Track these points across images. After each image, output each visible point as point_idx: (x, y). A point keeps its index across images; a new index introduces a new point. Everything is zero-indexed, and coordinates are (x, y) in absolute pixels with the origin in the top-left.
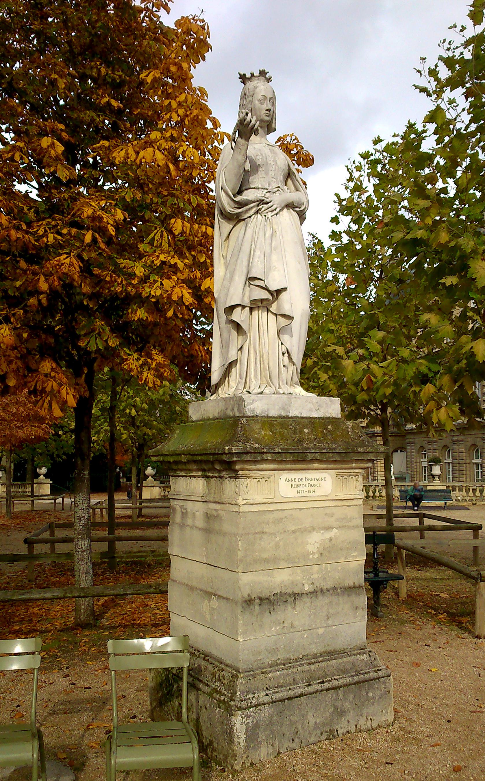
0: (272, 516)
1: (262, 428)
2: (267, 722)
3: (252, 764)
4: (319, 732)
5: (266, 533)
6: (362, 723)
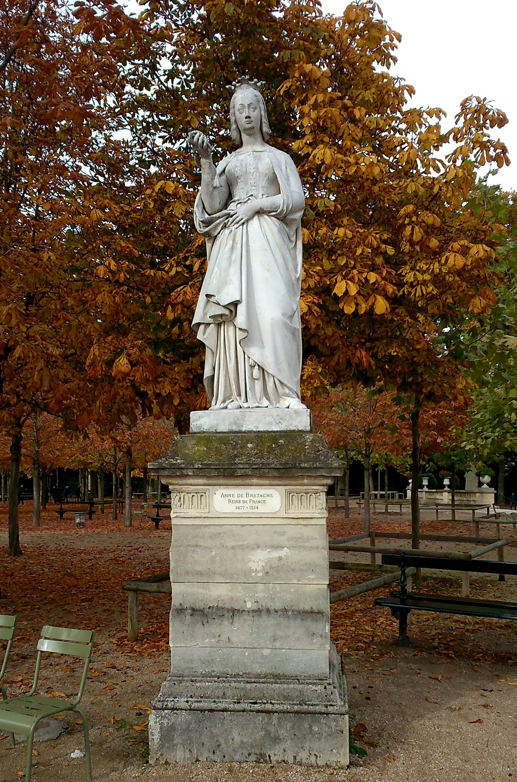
0: (207, 531)
1: (197, 444)
2: (184, 727)
3: (167, 763)
4: (246, 752)
5: (201, 546)
6: (303, 756)
